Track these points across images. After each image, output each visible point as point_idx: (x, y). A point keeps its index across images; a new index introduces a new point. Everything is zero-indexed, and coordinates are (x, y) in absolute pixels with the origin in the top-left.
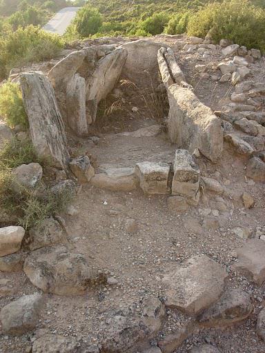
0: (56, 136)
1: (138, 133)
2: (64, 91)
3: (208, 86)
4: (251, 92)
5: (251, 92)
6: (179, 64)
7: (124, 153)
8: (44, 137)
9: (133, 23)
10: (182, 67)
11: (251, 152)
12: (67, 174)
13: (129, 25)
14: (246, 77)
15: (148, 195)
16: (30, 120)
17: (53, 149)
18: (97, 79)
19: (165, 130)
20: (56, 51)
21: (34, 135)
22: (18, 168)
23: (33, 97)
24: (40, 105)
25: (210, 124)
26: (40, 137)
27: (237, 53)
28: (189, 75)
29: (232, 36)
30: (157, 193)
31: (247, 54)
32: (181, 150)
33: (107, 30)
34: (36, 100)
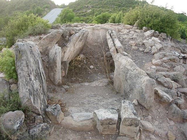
0: (37, 90)
1: (94, 84)
2: (47, 55)
3: (141, 54)
4: (165, 59)
5: (165, 59)
6: (119, 40)
7: (84, 98)
8: (27, 90)
9: (91, 18)
10: (122, 42)
11: (170, 101)
12: (43, 118)
13: (88, 19)
14: (160, 50)
15: (102, 134)
16: (19, 77)
17: (34, 99)
18: (69, 48)
19: (112, 83)
20: (45, 30)
21: (21, 88)
22: (6, 114)
23: (23, 60)
24: (27, 66)
25: (145, 83)
26: (24, 90)
27: (153, 35)
28: (127, 49)
29: (150, 25)
30: (109, 133)
31: (159, 36)
32: (125, 100)
33: (77, 21)
34: (24, 62)
